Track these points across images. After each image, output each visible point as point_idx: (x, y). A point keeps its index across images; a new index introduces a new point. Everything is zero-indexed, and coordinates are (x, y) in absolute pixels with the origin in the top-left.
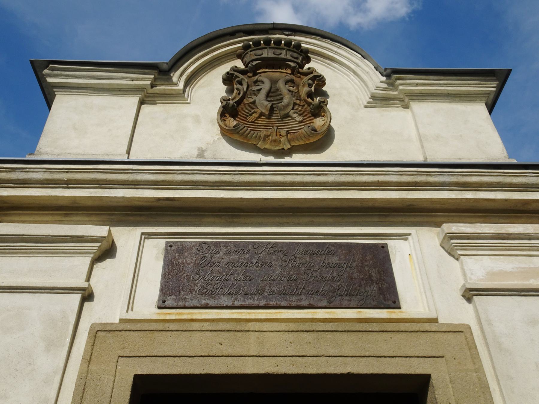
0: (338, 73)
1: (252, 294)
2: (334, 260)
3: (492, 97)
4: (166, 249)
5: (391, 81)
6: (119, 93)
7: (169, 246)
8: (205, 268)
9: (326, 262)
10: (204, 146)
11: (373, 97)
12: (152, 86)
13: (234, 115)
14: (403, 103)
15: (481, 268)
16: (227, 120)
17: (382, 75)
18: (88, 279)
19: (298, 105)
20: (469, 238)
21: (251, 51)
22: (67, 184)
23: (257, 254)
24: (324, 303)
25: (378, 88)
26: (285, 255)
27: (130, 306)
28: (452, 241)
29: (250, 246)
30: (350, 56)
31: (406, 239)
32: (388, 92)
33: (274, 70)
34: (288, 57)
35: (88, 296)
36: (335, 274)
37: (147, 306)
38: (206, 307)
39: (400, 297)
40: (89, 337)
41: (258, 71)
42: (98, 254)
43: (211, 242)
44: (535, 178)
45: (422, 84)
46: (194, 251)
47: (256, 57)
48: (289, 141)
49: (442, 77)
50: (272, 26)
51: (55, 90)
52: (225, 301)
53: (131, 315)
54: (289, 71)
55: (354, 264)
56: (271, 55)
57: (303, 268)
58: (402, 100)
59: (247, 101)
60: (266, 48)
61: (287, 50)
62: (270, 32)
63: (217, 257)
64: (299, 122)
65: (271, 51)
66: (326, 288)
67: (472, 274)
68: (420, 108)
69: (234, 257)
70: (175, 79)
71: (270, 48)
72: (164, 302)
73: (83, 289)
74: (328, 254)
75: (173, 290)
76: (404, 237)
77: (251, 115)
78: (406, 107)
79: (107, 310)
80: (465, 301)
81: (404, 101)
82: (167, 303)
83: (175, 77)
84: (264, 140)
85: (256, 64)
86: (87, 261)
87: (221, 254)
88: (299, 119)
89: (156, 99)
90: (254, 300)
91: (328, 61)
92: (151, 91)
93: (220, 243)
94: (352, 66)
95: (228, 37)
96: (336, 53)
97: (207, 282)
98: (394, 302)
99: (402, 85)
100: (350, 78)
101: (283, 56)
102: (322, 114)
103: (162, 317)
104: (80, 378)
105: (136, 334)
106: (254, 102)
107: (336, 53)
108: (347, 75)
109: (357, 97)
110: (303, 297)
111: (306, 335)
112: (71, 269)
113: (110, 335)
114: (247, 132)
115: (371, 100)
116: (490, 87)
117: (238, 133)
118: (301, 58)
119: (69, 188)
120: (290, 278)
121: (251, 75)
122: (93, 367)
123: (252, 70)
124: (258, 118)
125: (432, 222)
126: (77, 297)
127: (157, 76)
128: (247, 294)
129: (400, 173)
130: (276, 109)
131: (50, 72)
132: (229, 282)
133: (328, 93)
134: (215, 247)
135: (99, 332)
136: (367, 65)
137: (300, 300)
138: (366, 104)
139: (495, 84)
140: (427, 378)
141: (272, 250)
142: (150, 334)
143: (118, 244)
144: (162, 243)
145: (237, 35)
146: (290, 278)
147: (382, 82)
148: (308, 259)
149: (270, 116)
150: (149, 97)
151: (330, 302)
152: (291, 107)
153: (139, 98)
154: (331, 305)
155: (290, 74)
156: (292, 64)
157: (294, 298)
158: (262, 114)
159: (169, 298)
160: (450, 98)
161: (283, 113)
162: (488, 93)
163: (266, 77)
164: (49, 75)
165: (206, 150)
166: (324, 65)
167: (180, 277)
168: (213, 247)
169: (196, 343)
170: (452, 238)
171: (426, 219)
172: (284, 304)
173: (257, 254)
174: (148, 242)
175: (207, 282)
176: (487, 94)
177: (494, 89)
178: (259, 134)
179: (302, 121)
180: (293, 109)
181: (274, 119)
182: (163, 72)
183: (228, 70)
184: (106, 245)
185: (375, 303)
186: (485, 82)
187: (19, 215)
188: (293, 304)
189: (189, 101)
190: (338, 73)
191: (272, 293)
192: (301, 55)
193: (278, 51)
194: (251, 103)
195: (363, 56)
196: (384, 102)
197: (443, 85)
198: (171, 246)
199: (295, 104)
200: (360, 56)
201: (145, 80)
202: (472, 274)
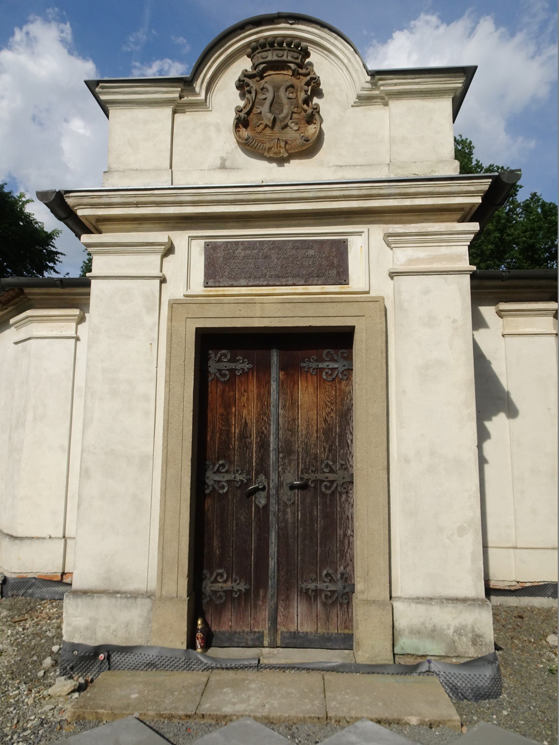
0: (334, 66)
1: (259, 278)
2: (311, 252)
3: (459, 92)
4: (205, 247)
5: (374, 81)
6: (156, 105)
7: (207, 245)
8: (230, 261)
9: (306, 254)
10: (225, 155)
11: (359, 97)
12: (181, 97)
13: (246, 126)
14: (384, 101)
15: (404, 256)
16: (240, 130)
17: (368, 75)
18: (161, 271)
19: (296, 113)
20: (400, 236)
21: (258, 53)
22: (137, 205)
23: (262, 249)
24: (302, 283)
25: (363, 89)
26: (280, 250)
27: (188, 286)
28: (389, 238)
29: (258, 244)
30: (344, 49)
31: (361, 235)
32: (371, 92)
33: (277, 72)
34: (290, 59)
35: (163, 280)
36: (311, 262)
37: (197, 285)
38: (232, 286)
39: (350, 277)
40: (169, 307)
41: (265, 75)
42: (164, 252)
43: (233, 242)
44: (457, 187)
45: (400, 83)
46: (222, 248)
47: (262, 60)
48: (287, 151)
49: (418, 76)
50: (277, 15)
51: (108, 106)
52: (243, 282)
53: (189, 293)
54: (290, 73)
55: (324, 255)
56: (275, 58)
57: (291, 259)
58: (382, 98)
59: (255, 111)
60: (270, 50)
61: (289, 50)
62: (276, 21)
63: (237, 252)
64: (296, 131)
65: (275, 52)
66: (304, 272)
67: (397, 261)
68: (398, 107)
69: (248, 252)
70: (197, 89)
71: (273, 50)
72: (207, 283)
73: (160, 277)
74: (308, 248)
75: (212, 275)
76: (359, 233)
77: (258, 126)
78: (386, 104)
79: (175, 290)
80: (390, 279)
81: (384, 99)
82: (209, 284)
83: (197, 85)
84: (268, 151)
85: (262, 69)
86: (159, 257)
87: (239, 250)
88: (296, 128)
89: (185, 108)
90: (260, 281)
91: (326, 53)
92: (180, 101)
93: (238, 242)
94: (346, 61)
95: (239, 32)
96: (333, 44)
97: (232, 270)
98: (345, 281)
99: (383, 85)
100: (343, 72)
101: (284, 58)
102: (315, 121)
103: (207, 293)
104: (168, 329)
105: (194, 305)
106: (261, 113)
107: (333, 44)
108: (342, 70)
109: (347, 94)
110: (290, 278)
111: (288, 305)
112: (150, 263)
113: (179, 306)
114: (255, 145)
115: (357, 100)
116: (458, 83)
117: (249, 145)
118: (300, 57)
119: (138, 207)
120: (282, 266)
121: (259, 79)
122: (174, 324)
123: (258, 74)
124: (264, 129)
125: (381, 220)
126: (157, 282)
127: (183, 88)
128: (255, 277)
129: (360, 188)
130: (277, 120)
131: (101, 90)
132: (245, 270)
133: (324, 92)
134: (236, 245)
135: (174, 304)
136: (357, 61)
137: (288, 281)
138: (353, 104)
139: (462, 80)
140: (353, 328)
141: (272, 246)
142: (201, 305)
143: (175, 244)
144: (202, 242)
145: (247, 28)
146: (282, 266)
147: (367, 82)
148: (294, 252)
149: (272, 128)
150: (179, 106)
151: (305, 282)
152: (289, 117)
153: (171, 109)
154: (307, 283)
155: (291, 76)
156: (292, 65)
157: (284, 280)
158: (266, 126)
159: (210, 281)
160: (423, 95)
161: (283, 124)
162: (456, 89)
163: (273, 77)
164: (101, 93)
165: (226, 160)
166: (323, 57)
167: (215, 267)
168: (234, 245)
169: (226, 311)
170: (389, 236)
171: (377, 219)
172: (278, 283)
173: (262, 249)
174: (194, 242)
175: (232, 270)
176: (454, 90)
177: (461, 85)
178: (265, 145)
179: (298, 130)
180: (291, 119)
181: (277, 128)
182: (186, 84)
183: (238, 74)
184: (168, 246)
185: (333, 281)
186: (451, 79)
187: (111, 224)
188: (283, 284)
189: (210, 109)
190: (334, 66)
191: (271, 276)
192: (300, 54)
193: (281, 53)
194: (258, 113)
195: (355, 50)
196: (368, 101)
197: (418, 83)
198: (208, 245)
199: (293, 113)
200: (352, 50)
201: (174, 93)
202: (397, 261)
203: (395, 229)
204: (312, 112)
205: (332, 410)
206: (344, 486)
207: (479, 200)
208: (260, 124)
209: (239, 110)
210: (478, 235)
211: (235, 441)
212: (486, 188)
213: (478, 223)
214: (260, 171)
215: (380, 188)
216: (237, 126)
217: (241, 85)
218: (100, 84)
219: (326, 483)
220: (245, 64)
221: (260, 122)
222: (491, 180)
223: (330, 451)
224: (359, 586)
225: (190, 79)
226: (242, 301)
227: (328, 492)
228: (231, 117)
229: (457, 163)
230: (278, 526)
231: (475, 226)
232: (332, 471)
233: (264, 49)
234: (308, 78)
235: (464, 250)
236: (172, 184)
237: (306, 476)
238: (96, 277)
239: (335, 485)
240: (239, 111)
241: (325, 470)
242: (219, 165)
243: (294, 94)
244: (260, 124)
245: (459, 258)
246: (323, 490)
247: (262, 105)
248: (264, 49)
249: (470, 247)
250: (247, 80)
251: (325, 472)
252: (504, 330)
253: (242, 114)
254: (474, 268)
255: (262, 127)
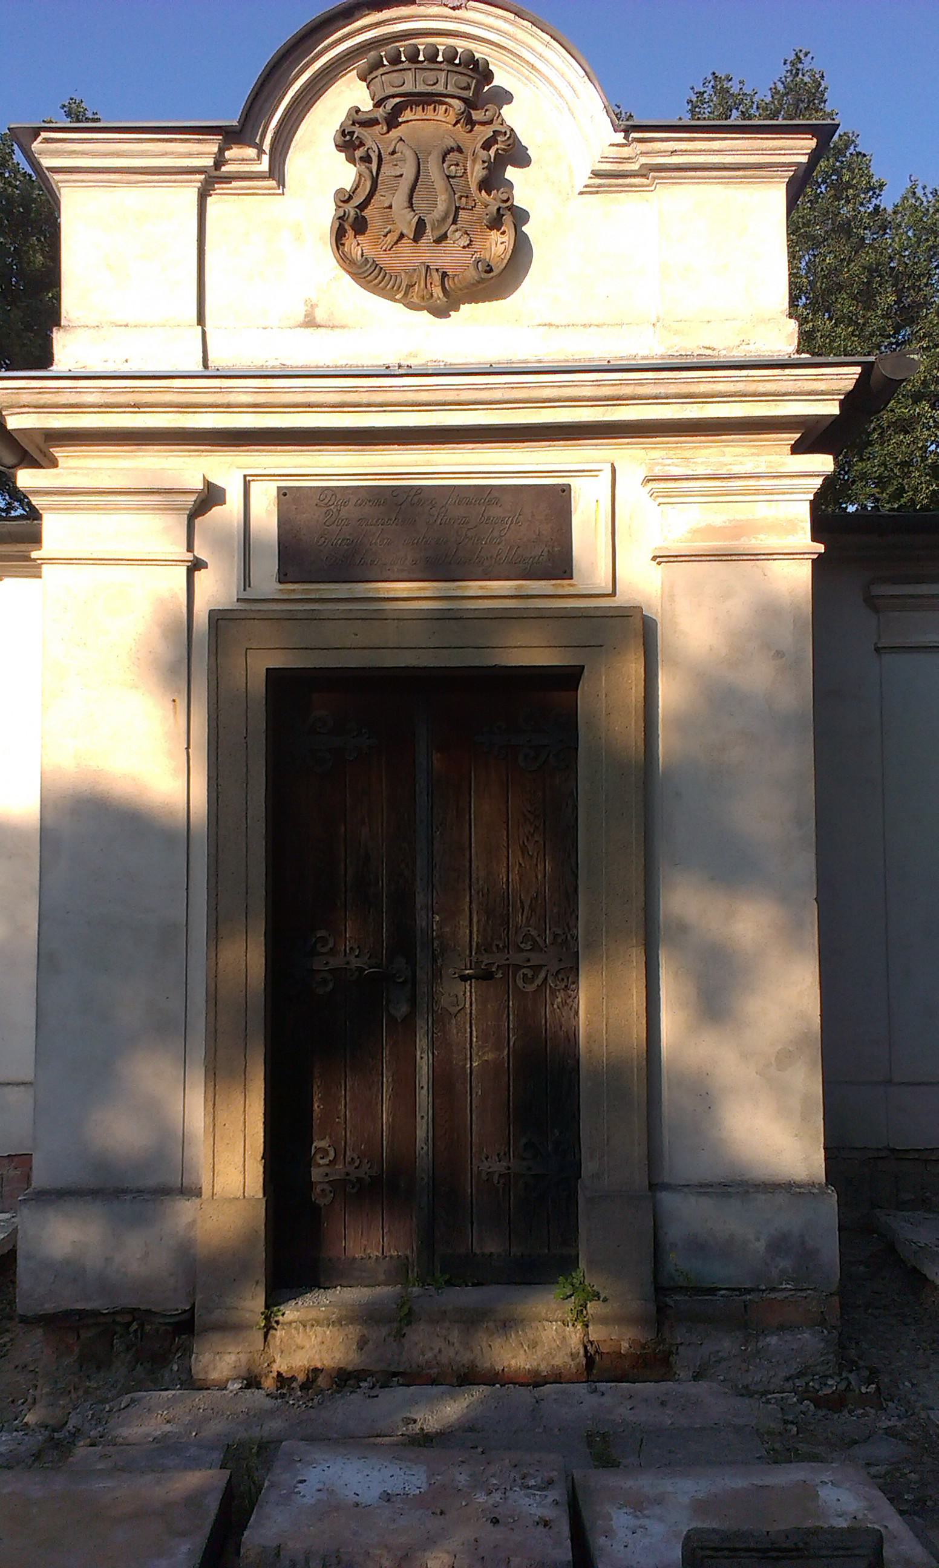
22: (137, 407)
34: (451, 89)
53: (250, 594)
64: (464, 247)
92: (217, 173)
106: (390, 207)
129: (598, 384)
152: (450, 220)
180: (454, 222)
193: (431, 76)
198: (285, 494)
203: (667, 468)
204: (499, 209)
205: (537, 828)
206: (560, 977)
207: (833, 409)
208: (389, 232)
209: (343, 198)
210: (829, 482)
211: (346, 891)
212: (849, 385)
213: (830, 458)
214: (389, 332)
215: (639, 383)
216: (339, 236)
217: (348, 142)
218: (44, 135)
219: (525, 971)
220: (352, 94)
221: (389, 227)
222: (858, 370)
223: (532, 909)
224: (589, 1167)
225: (238, 129)
226: (359, 615)
227: (531, 988)
228: (327, 213)
229: (793, 325)
230: (433, 1054)
231: (824, 463)
232: (535, 948)
233: (396, 68)
234: (488, 132)
235: (803, 513)
236: (206, 365)
237: (486, 959)
238: (51, 560)
239: (542, 975)
240: (344, 202)
241: (522, 946)
242: (301, 318)
243: (460, 167)
244: (389, 232)
245: (789, 527)
246: (520, 983)
247: (394, 190)
248: (396, 68)
249: (815, 505)
250: (358, 131)
251: (522, 950)
252: (879, 638)
253: (350, 209)
254: (821, 548)
255: (394, 236)
